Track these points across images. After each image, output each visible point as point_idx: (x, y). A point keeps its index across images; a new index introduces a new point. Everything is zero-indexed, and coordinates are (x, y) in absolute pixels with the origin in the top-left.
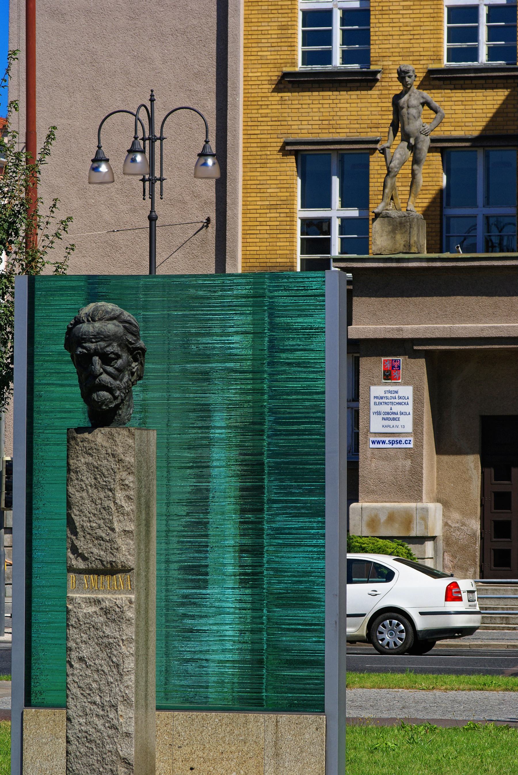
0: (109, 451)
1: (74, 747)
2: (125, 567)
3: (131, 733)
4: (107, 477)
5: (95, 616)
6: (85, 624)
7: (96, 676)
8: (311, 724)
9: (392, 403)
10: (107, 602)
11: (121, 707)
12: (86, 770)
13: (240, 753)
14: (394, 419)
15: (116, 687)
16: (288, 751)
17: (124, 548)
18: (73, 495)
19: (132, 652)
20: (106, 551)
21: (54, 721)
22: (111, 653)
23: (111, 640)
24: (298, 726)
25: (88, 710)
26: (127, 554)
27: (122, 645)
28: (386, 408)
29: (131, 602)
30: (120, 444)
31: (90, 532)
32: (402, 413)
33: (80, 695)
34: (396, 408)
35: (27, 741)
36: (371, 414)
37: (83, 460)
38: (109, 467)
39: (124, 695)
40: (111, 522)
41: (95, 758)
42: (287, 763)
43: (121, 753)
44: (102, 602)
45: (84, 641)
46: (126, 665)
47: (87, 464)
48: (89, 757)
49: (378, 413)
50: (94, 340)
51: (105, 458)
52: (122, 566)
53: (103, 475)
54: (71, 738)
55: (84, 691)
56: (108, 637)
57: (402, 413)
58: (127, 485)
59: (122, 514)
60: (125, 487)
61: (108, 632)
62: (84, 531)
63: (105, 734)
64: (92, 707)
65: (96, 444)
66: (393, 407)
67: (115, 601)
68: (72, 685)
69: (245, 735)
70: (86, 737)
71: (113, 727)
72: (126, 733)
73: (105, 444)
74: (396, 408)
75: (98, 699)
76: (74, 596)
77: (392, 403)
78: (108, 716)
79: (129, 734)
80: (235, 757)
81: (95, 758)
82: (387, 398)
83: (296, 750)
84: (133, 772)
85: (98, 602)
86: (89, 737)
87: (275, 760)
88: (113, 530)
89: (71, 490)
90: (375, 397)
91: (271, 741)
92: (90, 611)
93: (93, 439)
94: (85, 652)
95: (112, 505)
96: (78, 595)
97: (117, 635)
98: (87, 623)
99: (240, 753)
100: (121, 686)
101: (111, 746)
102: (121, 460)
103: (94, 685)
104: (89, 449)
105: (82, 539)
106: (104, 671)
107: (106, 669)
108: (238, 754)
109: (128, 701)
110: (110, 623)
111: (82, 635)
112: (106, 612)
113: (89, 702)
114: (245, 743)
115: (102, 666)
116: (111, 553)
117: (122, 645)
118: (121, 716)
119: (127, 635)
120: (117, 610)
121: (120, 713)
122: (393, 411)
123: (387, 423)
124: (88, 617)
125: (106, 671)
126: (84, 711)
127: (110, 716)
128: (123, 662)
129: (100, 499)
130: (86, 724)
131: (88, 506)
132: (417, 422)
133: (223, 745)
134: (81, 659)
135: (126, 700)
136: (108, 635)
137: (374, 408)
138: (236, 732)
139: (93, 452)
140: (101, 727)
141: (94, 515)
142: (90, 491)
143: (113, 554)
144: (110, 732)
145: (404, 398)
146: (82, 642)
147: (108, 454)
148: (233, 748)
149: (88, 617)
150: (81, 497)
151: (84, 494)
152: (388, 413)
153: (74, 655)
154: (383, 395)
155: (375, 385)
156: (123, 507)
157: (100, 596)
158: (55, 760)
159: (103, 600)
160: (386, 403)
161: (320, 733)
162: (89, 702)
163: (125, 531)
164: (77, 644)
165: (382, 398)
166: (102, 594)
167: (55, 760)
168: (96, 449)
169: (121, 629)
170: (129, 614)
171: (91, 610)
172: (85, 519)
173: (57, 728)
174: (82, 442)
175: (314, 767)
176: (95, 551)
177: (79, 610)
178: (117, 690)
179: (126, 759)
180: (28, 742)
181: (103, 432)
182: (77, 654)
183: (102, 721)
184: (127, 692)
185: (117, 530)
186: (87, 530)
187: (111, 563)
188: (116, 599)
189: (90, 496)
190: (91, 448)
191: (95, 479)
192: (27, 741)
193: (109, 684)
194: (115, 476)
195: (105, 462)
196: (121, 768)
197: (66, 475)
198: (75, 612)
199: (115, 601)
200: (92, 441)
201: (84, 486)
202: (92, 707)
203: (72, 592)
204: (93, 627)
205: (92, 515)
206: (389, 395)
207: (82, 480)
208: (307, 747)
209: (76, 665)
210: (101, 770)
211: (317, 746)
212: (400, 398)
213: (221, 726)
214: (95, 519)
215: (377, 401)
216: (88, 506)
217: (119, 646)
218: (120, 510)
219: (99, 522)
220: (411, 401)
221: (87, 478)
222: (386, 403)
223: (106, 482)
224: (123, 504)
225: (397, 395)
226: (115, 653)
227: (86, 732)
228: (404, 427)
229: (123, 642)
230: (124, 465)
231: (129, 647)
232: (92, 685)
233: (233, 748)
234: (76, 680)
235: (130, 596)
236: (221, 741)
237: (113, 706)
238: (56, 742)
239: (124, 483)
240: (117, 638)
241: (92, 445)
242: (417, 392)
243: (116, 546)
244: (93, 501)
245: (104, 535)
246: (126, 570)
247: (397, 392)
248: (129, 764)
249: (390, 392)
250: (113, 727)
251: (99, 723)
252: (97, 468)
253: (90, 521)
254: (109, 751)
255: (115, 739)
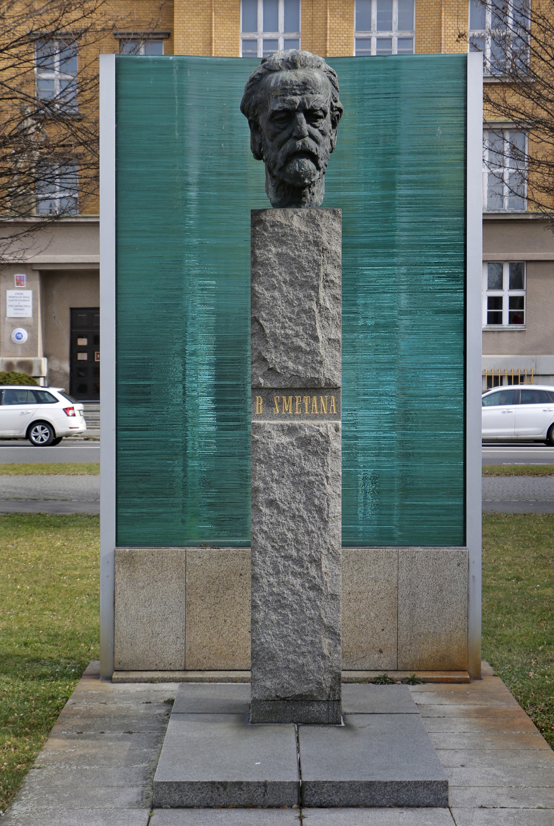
0: (311, 238)
1: (262, 614)
2: (330, 384)
3: (337, 594)
4: (308, 271)
5: (291, 447)
6: (277, 458)
7: (292, 524)
8: (452, 559)
9: (20, 300)
10: (306, 430)
11: (325, 562)
12: (278, 642)
13: (370, 593)
14: (21, 309)
15: (318, 537)
16: (425, 589)
17: (328, 361)
18: (261, 294)
19: (338, 492)
20: (305, 365)
21: (152, 562)
22: (312, 493)
23: (312, 478)
24: (436, 561)
25: (281, 567)
26: (332, 369)
27: (326, 484)
28: (16, 303)
29: (337, 430)
30: (323, 229)
31: (285, 341)
32: (25, 306)
33: (270, 549)
34: (22, 303)
35: (120, 585)
36: (7, 307)
37: (273, 249)
38: (311, 259)
39: (330, 547)
40: (315, 329)
41: (291, 627)
42: (424, 603)
43: (325, 619)
44: (299, 430)
45: (276, 480)
46: (332, 509)
47: (278, 255)
48: (283, 625)
49: (12, 306)
50: (298, 92)
51: (305, 247)
52: (326, 384)
53: (301, 268)
54: (259, 602)
55: (276, 543)
56: (308, 474)
57: (25, 306)
58: (332, 281)
59: (326, 318)
60: (329, 284)
61: (308, 467)
62: (275, 340)
63: (304, 597)
64: (286, 563)
65: (292, 230)
66: (20, 302)
67: (318, 428)
68: (259, 536)
69: (375, 573)
70: (280, 601)
71: (315, 588)
72: (331, 594)
73: (304, 229)
74: (22, 303)
75: (294, 553)
76: (262, 422)
77: (20, 300)
78: (308, 573)
79: (336, 595)
80: (364, 597)
81: (291, 627)
82: (16, 297)
83: (434, 588)
84: (340, 643)
85: (291, 430)
86: (282, 602)
87: (411, 600)
88: (316, 339)
89: (259, 289)
90: (10, 297)
91: (405, 579)
92: (283, 441)
93: (287, 223)
94: (277, 493)
95: (314, 307)
96: (266, 422)
97: (320, 470)
98: (280, 457)
99: (370, 593)
100: (326, 536)
101: (313, 612)
102: (326, 250)
103: (290, 535)
104: (282, 236)
105: (273, 350)
106: (301, 517)
107: (305, 514)
108: (368, 595)
109: (334, 554)
110: (311, 457)
111: (273, 471)
112: (304, 442)
113: (282, 557)
114: (375, 582)
115: (298, 510)
116: (312, 368)
117: (326, 484)
118: (325, 573)
119: (332, 471)
120: (321, 440)
121: (324, 569)
122: (21, 304)
123: (17, 311)
124: (281, 449)
125: (305, 516)
126: (275, 565)
127: (312, 574)
128: (328, 505)
129: (299, 299)
130: (278, 584)
131: (282, 308)
132: (34, 312)
133: (350, 585)
134: (271, 503)
135: (331, 553)
136: (309, 472)
137: (8, 303)
138: (365, 570)
139: (288, 240)
140: (298, 587)
141: (290, 319)
142: (285, 289)
143: (315, 369)
144: (312, 594)
145: (27, 297)
146: (272, 481)
147: (309, 241)
148: (362, 588)
149: (281, 449)
150: (272, 296)
151: (277, 294)
152: (17, 306)
153: (261, 497)
154: (14, 295)
155: (9, 289)
156: (328, 309)
157: (296, 422)
158: (153, 606)
159: (300, 427)
160: (16, 300)
161: (462, 569)
162: (282, 557)
163: (330, 339)
164: (266, 483)
165: (13, 297)
166: (298, 420)
167: (153, 606)
168: (291, 235)
169: (326, 464)
170: (335, 444)
171: (285, 440)
172: (277, 325)
173: (156, 570)
174: (272, 226)
175: (456, 607)
176: (290, 365)
177: (270, 440)
178: (320, 541)
179: (331, 627)
180: (121, 587)
181: (300, 214)
182: (266, 497)
183: (299, 581)
184: (333, 543)
185: (321, 338)
186: (280, 338)
187: (313, 379)
188: (318, 426)
189: (283, 295)
190: (285, 235)
191: (291, 273)
192: (120, 585)
193: (309, 533)
194: (319, 269)
195: (304, 252)
196: (325, 639)
197: (249, 268)
198: (264, 443)
199: (318, 428)
200: (286, 225)
201: (275, 282)
202: (286, 563)
203: (259, 417)
204: (288, 461)
205: (287, 320)
206: (18, 296)
207: (274, 276)
208: (447, 585)
209: (265, 510)
210: (299, 642)
211: (458, 584)
212: (24, 297)
213: (348, 563)
214: (291, 324)
215: (11, 299)
216: (282, 308)
217: (323, 485)
218: (323, 313)
219: (297, 328)
220: (31, 299)
221: (280, 274)
222: (16, 300)
223: (305, 277)
224: (328, 305)
225: (22, 296)
226: (318, 493)
227: (278, 595)
228: (26, 314)
229: (327, 480)
230: (329, 255)
231: (335, 485)
232: (286, 535)
233: (363, 588)
234: (265, 528)
235: (336, 422)
236: (348, 580)
237: (315, 561)
238: (154, 586)
239: (328, 279)
240: (321, 475)
241: (288, 231)
242: (34, 294)
243: (319, 358)
244: (289, 303)
245: (303, 345)
246: (331, 388)
247: (22, 294)
248: (335, 633)
249: (18, 294)
250: (315, 588)
251: (297, 582)
252: (293, 259)
253: (285, 328)
254: (310, 619)
255: (318, 603)
